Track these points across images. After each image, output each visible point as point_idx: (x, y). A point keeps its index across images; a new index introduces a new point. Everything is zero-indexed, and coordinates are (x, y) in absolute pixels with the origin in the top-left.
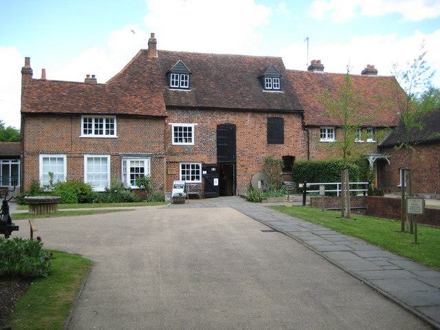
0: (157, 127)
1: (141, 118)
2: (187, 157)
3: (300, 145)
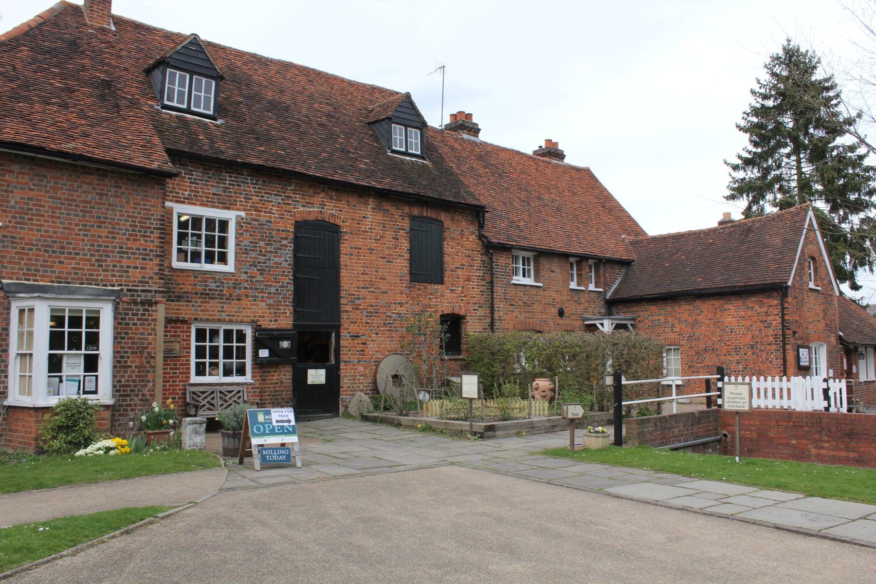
0: (127, 206)
1: (86, 171)
2: (213, 306)
3: (476, 289)
